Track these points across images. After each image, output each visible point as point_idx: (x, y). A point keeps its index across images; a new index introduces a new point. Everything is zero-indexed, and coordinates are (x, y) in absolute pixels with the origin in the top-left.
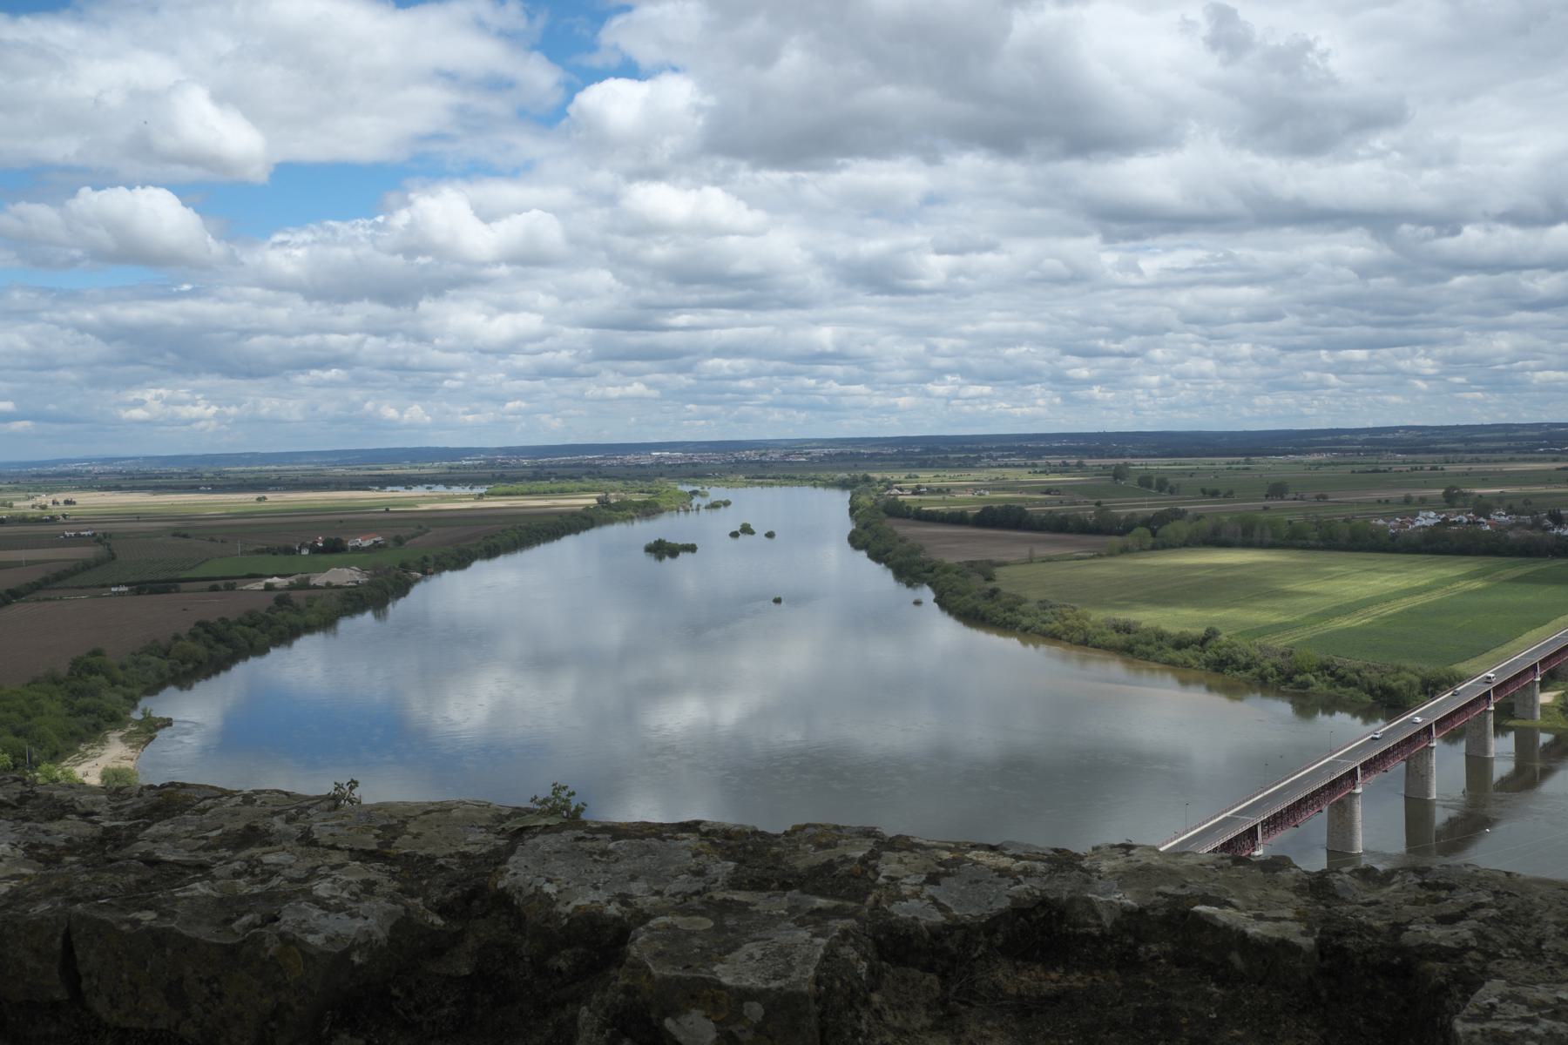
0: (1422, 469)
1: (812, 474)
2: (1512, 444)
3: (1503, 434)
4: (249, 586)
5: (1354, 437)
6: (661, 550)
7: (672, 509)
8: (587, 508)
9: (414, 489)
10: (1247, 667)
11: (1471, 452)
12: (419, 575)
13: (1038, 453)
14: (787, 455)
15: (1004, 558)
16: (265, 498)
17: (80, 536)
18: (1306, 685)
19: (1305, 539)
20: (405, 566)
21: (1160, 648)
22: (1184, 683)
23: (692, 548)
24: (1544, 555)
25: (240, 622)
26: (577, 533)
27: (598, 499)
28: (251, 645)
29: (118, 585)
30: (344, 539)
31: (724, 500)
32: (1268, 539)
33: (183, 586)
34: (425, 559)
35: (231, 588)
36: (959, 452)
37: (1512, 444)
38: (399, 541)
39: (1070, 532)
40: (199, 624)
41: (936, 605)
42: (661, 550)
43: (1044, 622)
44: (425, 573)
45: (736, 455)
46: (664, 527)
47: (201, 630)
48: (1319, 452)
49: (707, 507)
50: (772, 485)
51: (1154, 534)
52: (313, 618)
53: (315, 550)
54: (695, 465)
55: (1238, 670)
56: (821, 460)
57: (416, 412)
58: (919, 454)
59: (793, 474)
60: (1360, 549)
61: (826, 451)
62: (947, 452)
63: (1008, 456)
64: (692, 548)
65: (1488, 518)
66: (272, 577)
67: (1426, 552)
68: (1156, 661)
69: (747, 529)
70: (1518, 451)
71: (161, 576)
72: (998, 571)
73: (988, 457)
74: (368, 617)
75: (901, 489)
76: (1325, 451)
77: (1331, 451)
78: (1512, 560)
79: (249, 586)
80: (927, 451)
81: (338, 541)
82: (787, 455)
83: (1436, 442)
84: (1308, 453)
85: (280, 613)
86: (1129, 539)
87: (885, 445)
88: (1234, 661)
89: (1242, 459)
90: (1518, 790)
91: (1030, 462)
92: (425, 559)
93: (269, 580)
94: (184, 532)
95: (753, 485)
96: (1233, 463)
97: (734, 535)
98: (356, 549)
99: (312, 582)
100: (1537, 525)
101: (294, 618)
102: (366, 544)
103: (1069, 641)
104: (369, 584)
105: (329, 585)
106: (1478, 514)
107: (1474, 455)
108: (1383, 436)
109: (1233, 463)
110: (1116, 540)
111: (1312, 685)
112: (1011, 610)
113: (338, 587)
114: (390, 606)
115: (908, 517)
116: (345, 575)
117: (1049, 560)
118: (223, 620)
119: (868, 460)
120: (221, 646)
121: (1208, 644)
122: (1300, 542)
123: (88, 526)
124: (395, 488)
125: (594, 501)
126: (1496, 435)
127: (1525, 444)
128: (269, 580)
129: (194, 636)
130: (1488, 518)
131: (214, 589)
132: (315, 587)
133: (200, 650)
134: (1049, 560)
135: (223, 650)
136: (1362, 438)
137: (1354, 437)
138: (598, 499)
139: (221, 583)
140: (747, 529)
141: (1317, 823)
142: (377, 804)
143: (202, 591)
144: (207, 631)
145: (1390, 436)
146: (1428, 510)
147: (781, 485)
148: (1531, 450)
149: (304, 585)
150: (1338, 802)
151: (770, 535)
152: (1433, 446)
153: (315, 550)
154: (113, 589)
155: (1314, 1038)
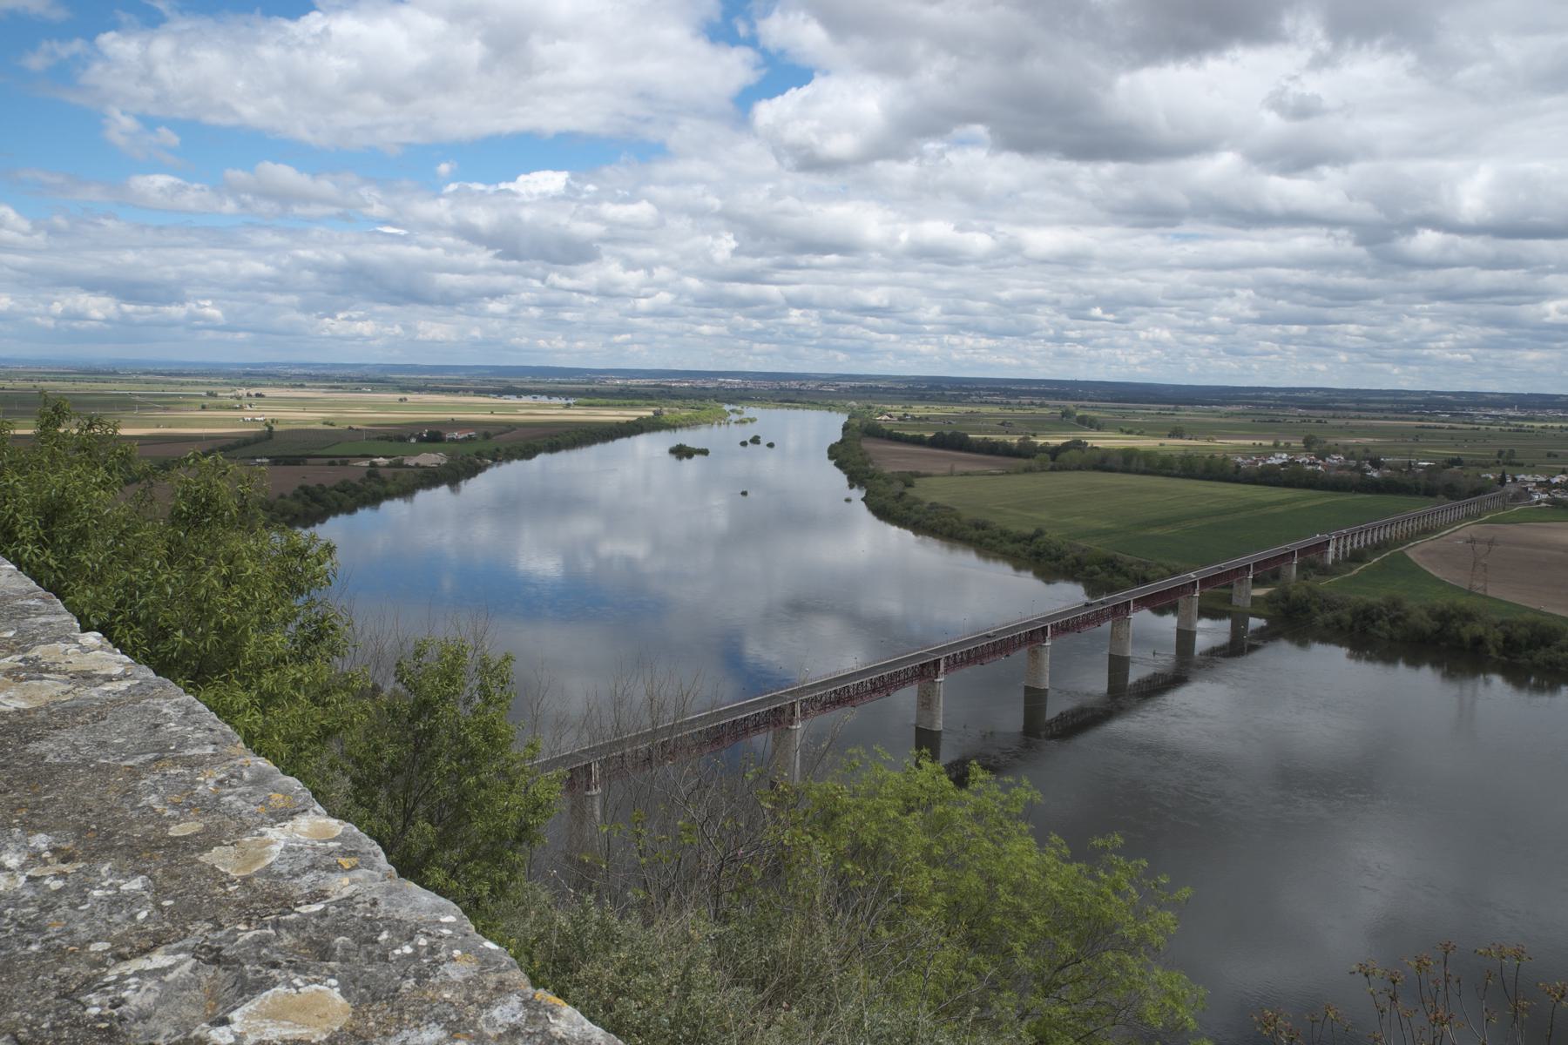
0: (1309, 421)
1: (830, 401)
2: (1395, 406)
3: (1392, 398)
4: (359, 464)
5: (1273, 394)
6: (681, 452)
7: (708, 422)
8: (648, 418)
9: (524, 398)
10: (1057, 559)
11: (1358, 410)
12: (490, 461)
13: (1016, 394)
14: (821, 386)
15: (928, 471)
16: (406, 399)
17: (254, 420)
18: (1093, 573)
19: (1171, 468)
20: (479, 455)
21: (1001, 541)
22: (1018, 568)
23: (705, 452)
24: (1350, 491)
25: (335, 488)
26: (629, 437)
27: (654, 411)
28: (340, 505)
29: (261, 458)
30: (443, 431)
31: (751, 417)
32: (1142, 467)
33: (309, 460)
34: (498, 450)
35: (344, 464)
36: (955, 390)
37: (1395, 406)
38: (487, 436)
39: (999, 454)
40: (301, 488)
41: (863, 503)
42: (681, 452)
43: (928, 519)
44: (495, 460)
45: (782, 383)
46: (687, 438)
47: (301, 492)
48: (1238, 404)
49: (736, 423)
50: (797, 408)
51: (1053, 459)
52: (391, 488)
53: (420, 439)
54: (746, 390)
55: (1051, 560)
56: (846, 390)
57: (559, 343)
58: (925, 390)
59: (815, 401)
60: (1211, 479)
61: (853, 384)
62: (946, 389)
63: (994, 395)
64: (705, 452)
65: (1324, 461)
66: (378, 457)
67: (1261, 484)
68: (997, 551)
69: (756, 440)
70: (1396, 411)
71: (298, 454)
72: (917, 481)
73: (976, 395)
74: (444, 490)
75: (890, 416)
76: (1243, 404)
77: (1248, 404)
78: (1329, 493)
79: (359, 464)
80: (931, 388)
81: (439, 434)
82: (821, 386)
83: (1336, 401)
84: (1230, 404)
85: (368, 483)
86: (1032, 462)
87: (899, 382)
88: (1049, 554)
89: (1172, 406)
90: (1225, 656)
91: (1005, 401)
92: (498, 450)
93: (375, 460)
94: (331, 422)
95: (783, 407)
96: (1164, 409)
97: (744, 444)
98: (453, 440)
99: (405, 462)
100: (1358, 468)
101: (377, 487)
102: (461, 437)
103: (941, 533)
104: (445, 466)
105: (417, 465)
106: (1318, 457)
107: (1357, 413)
108: (1297, 394)
109: (1164, 409)
110: (1023, 462)
111: (1097, 574)
112: (909, 509)
113: (423, 467)
114: (462, 483)
115: (882, 437)
116: (431, 459)
117: (967, 474)
118: (320, 486)
119: (883, 393)
120: (316, 506)
121: (1035, 540)
122: (1165, 471)
123: (261, 413)
124: (507, 397)
125: (651, 414)
126: (1387, 398)
127: (1405, 406)
128: (375, 460)
129: (296, 496)
130: (1324, 461)
131: (332, 464)
132: (407, 466)
133: (297, 506)
134: (967, 474)
135: (317, 507)
136: (1281, 394)
137: (1273, 394)
138: (654, 411)
139: (337, 460)
140: (756, 440)
141: (907, 697)
142: (929, 540)
143: (322, 465)
144: (306, 493)
145: (1302, 395)
146: (1282, 453)
147: (804, 408)
148: (1407, 411)
149: (400, 465)
150: (775, 709)
151: (771, 445)
152: (1331, 404)
153: (420, 439)
154: (258, 460)
155: (155, 991)
